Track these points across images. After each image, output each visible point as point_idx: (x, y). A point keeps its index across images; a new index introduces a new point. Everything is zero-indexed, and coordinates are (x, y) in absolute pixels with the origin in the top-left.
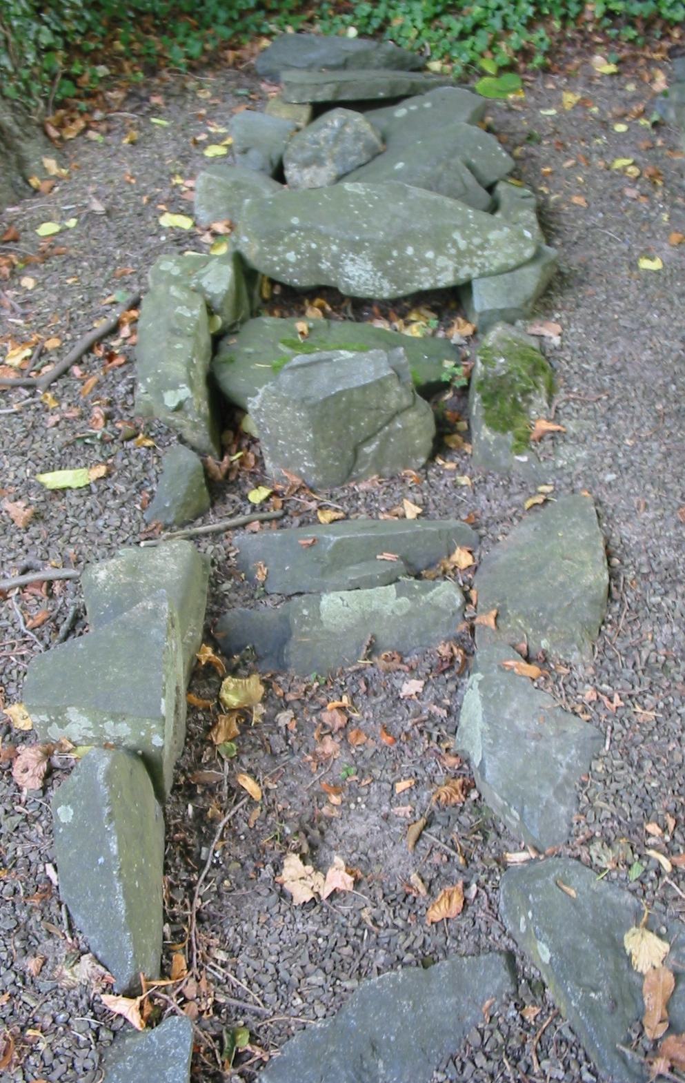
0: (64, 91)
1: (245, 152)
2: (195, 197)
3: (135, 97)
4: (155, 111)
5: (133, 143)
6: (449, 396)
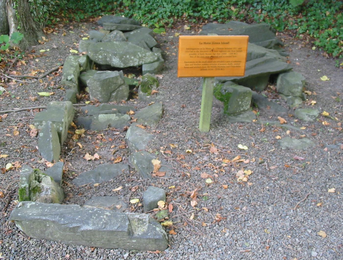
0: (48, 22)
1: (92, 39)
2: (79, 47)
3: (66, 26)
4: (71, 29)
5: (65, 36)
6: (135, 89)
